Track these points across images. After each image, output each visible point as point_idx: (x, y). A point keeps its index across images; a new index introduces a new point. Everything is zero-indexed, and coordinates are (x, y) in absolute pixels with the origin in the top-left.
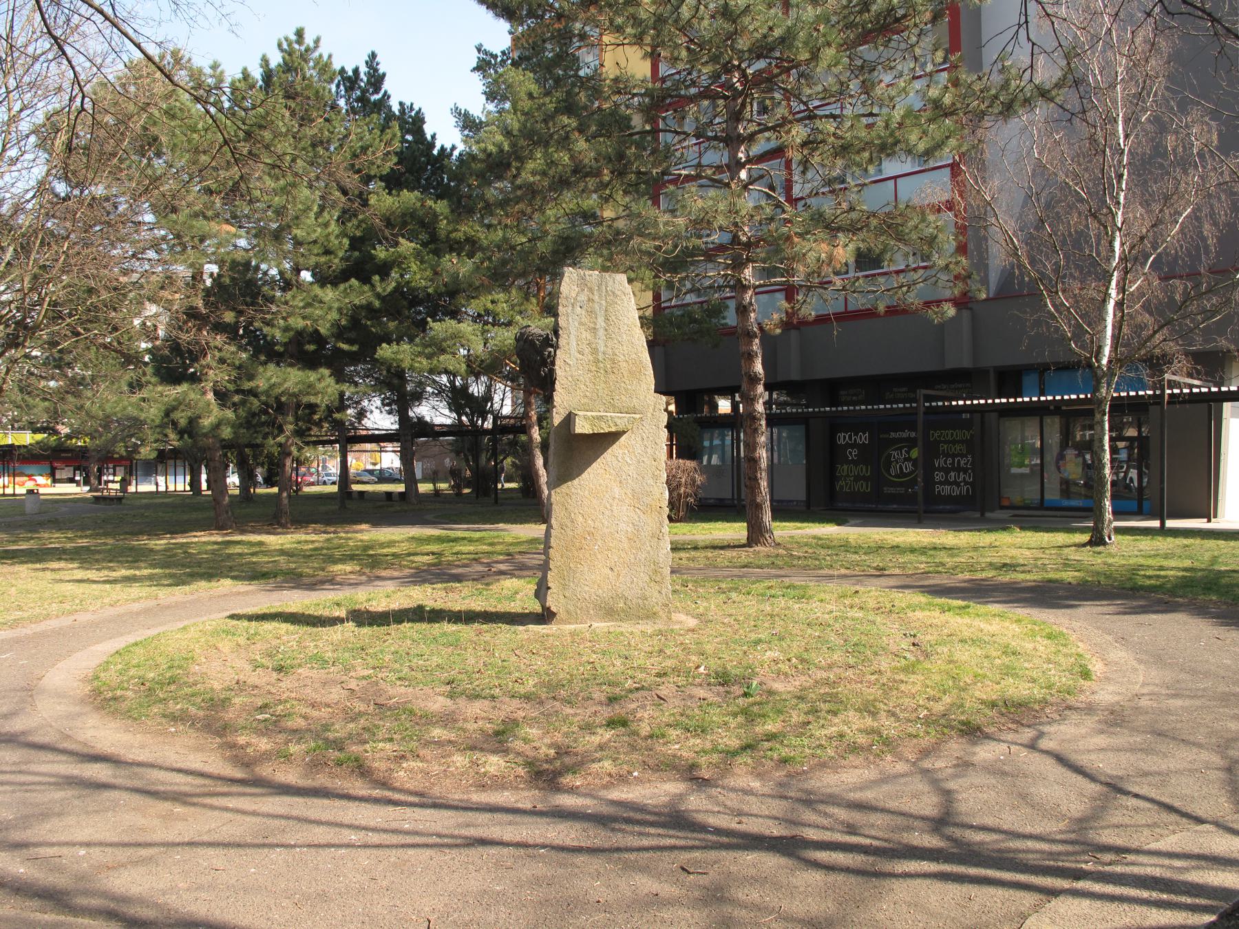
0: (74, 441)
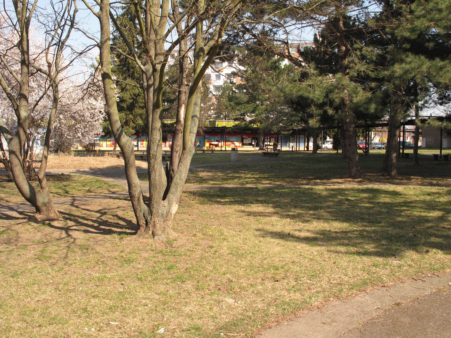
0: (252, 125)
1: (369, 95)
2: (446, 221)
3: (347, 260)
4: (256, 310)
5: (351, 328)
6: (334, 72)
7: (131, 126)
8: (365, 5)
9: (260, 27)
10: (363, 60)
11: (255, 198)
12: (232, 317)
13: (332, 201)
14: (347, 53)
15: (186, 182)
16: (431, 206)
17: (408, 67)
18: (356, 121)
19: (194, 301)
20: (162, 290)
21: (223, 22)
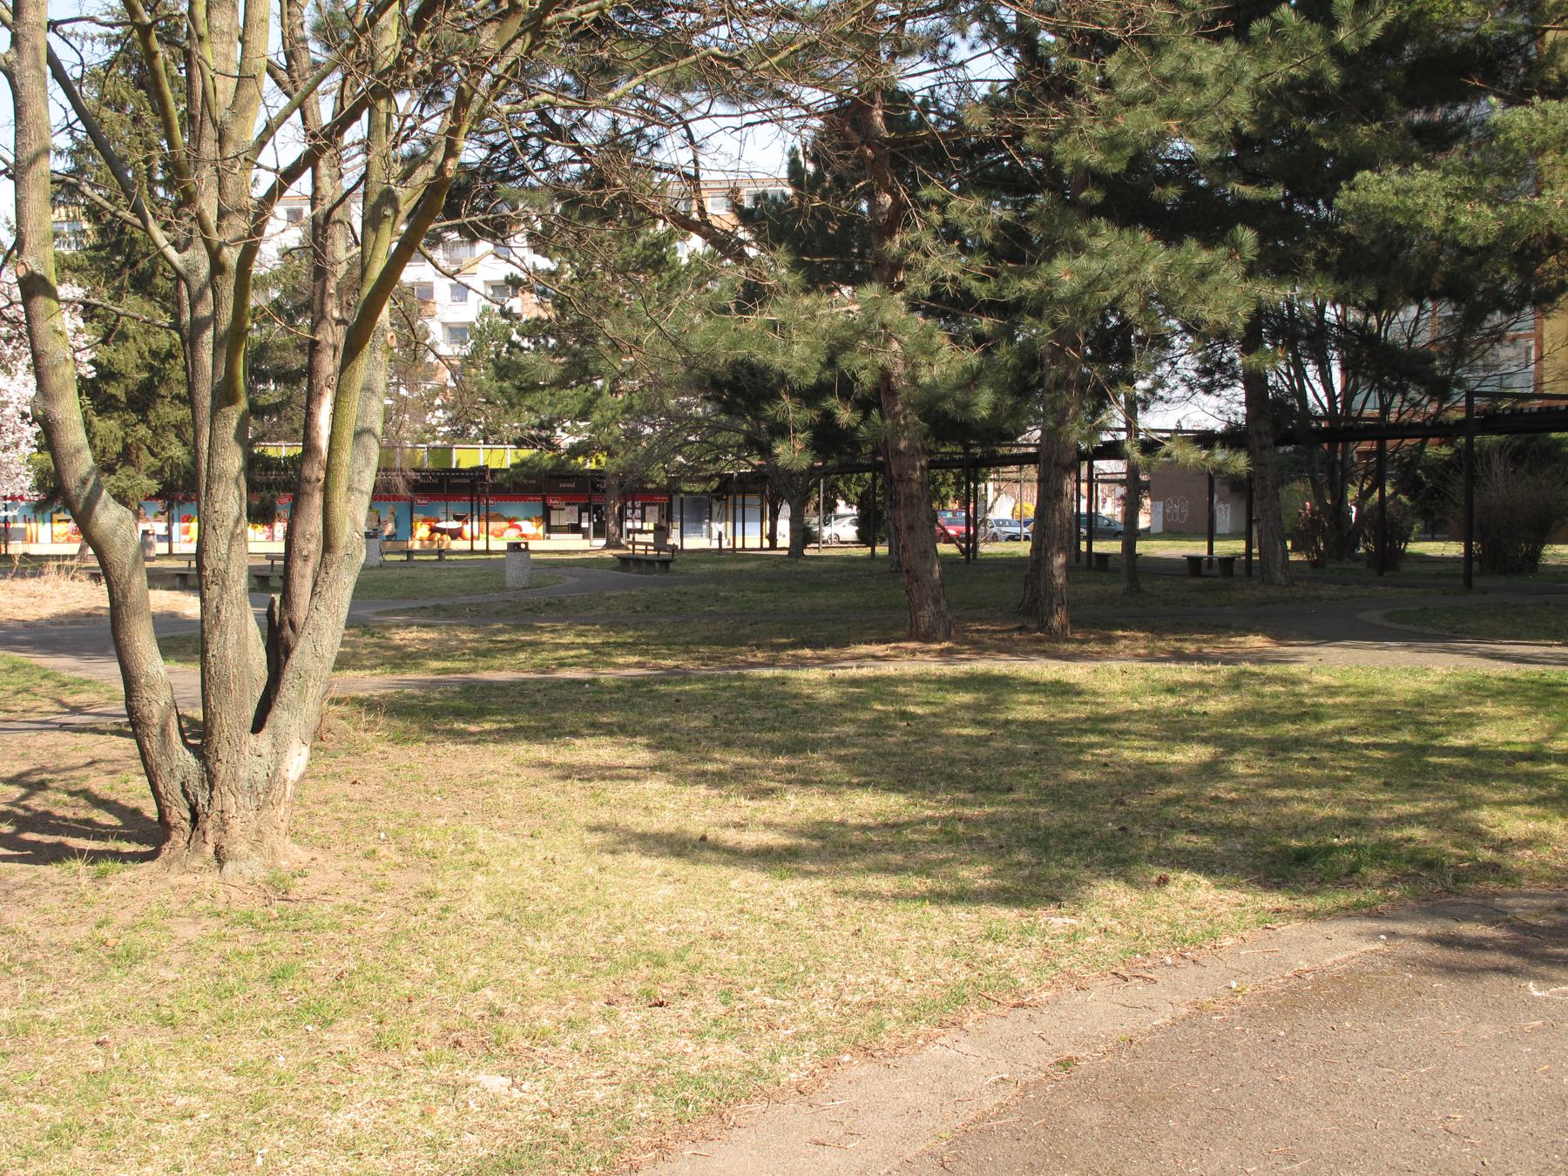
0: (580, 460)
1: (972, 358)
2: (1224, 779)
3: (899, 920)
4: (586, 1110)
5: (908, 1156)
6: (856, 280)
7: (143, 468)
8: (957, 55)
9: (600, 121)
10: (950, 241)
11: (589, 717)
12: (500, 1141)
13: (852, 721)
14: (898, 218)
15: (334, 669)
16: (1177, 729)
17: (1096, 266)
18: (932, 447)
19: (366, 1090)
20: (250, 1057)
21: (463, 101)
